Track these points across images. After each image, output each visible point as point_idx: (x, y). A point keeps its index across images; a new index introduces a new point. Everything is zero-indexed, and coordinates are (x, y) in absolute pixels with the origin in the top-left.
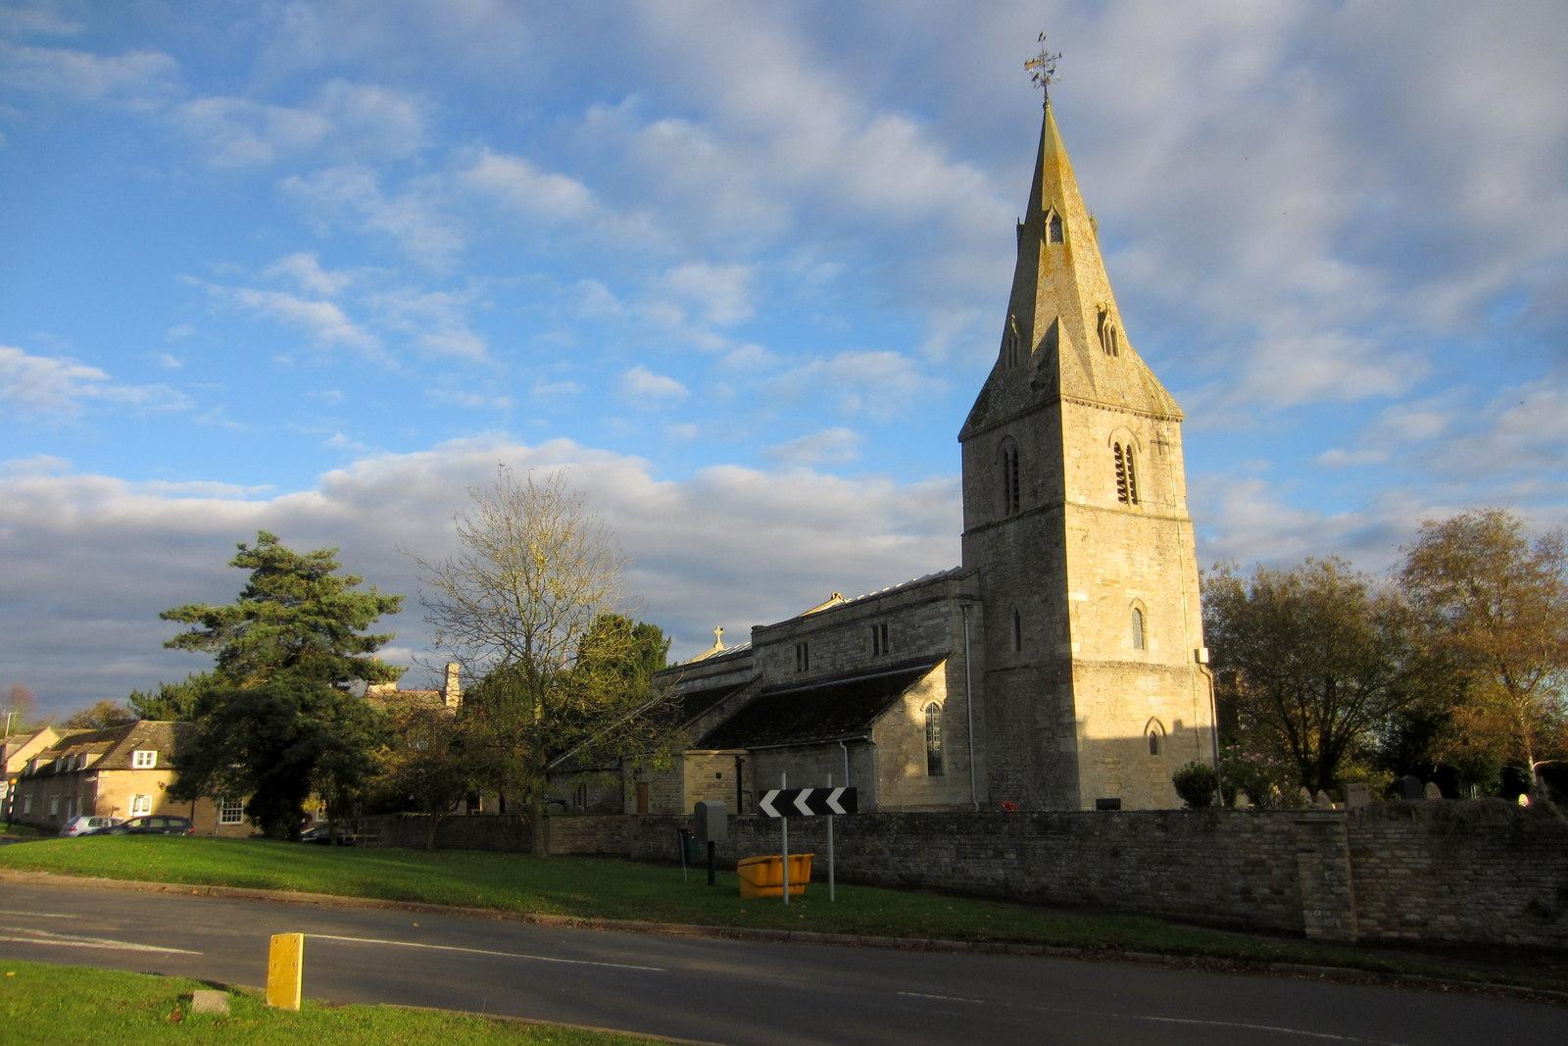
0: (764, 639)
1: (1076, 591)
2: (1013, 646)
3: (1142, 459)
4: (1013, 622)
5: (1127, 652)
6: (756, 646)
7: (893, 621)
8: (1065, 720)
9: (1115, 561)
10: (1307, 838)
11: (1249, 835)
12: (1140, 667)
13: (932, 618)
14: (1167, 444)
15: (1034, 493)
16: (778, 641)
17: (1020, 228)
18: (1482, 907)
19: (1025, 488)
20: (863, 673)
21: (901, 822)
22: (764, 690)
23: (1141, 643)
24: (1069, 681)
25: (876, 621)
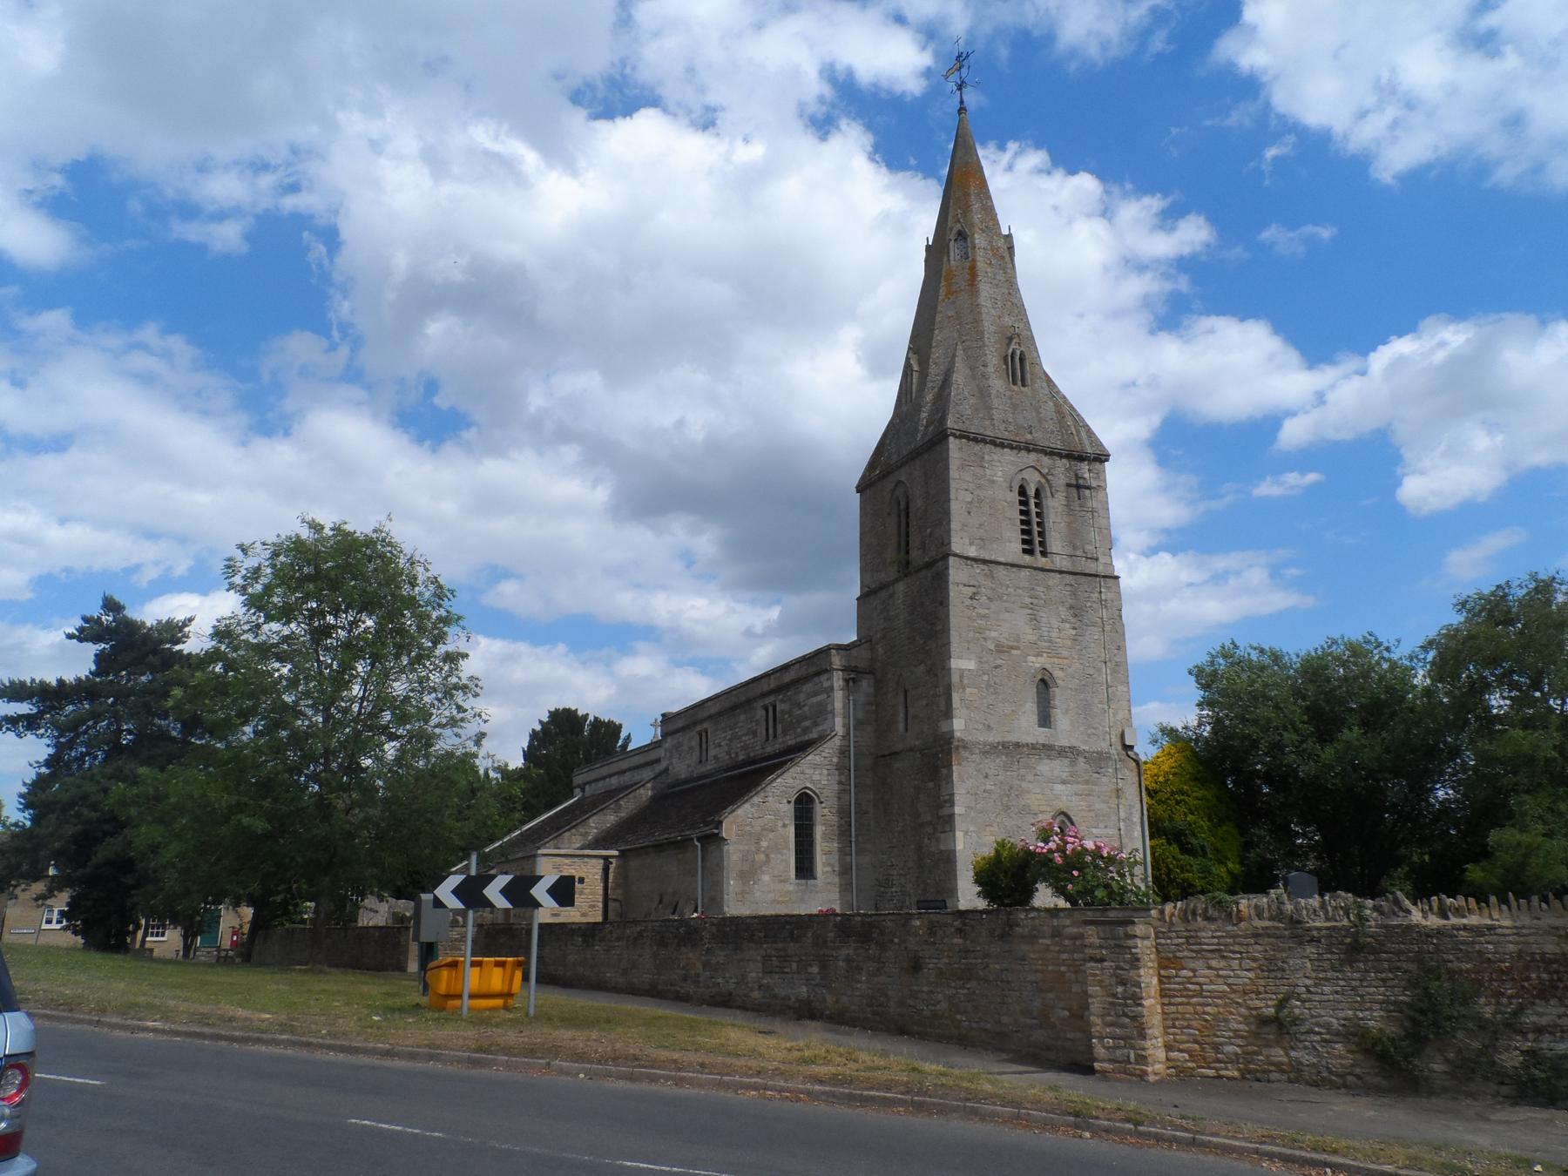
0: (671, 727)
1: (960, 658)
2: (901, 726)
3: (1055, 506)
4: (901, 697)
5: (1026, 727)
6: (664, 735)
7: (782, 701)
8: (945, 811)
9: (1013, 624)
10: (1097, 941)
11: (1047, 942)
12: (1048, 750)
13: (816, 694)
14: (1088, 488)
15: (923, 546)
16: (683, 729)
17: (928, 248)
18: (1317, 1038)
19: (915, 541)
20: (754, 762)
21: (714, 929)
22: (671, 786)
23: (1045, 720)
24: (949, 766)
25: (767, 701)
